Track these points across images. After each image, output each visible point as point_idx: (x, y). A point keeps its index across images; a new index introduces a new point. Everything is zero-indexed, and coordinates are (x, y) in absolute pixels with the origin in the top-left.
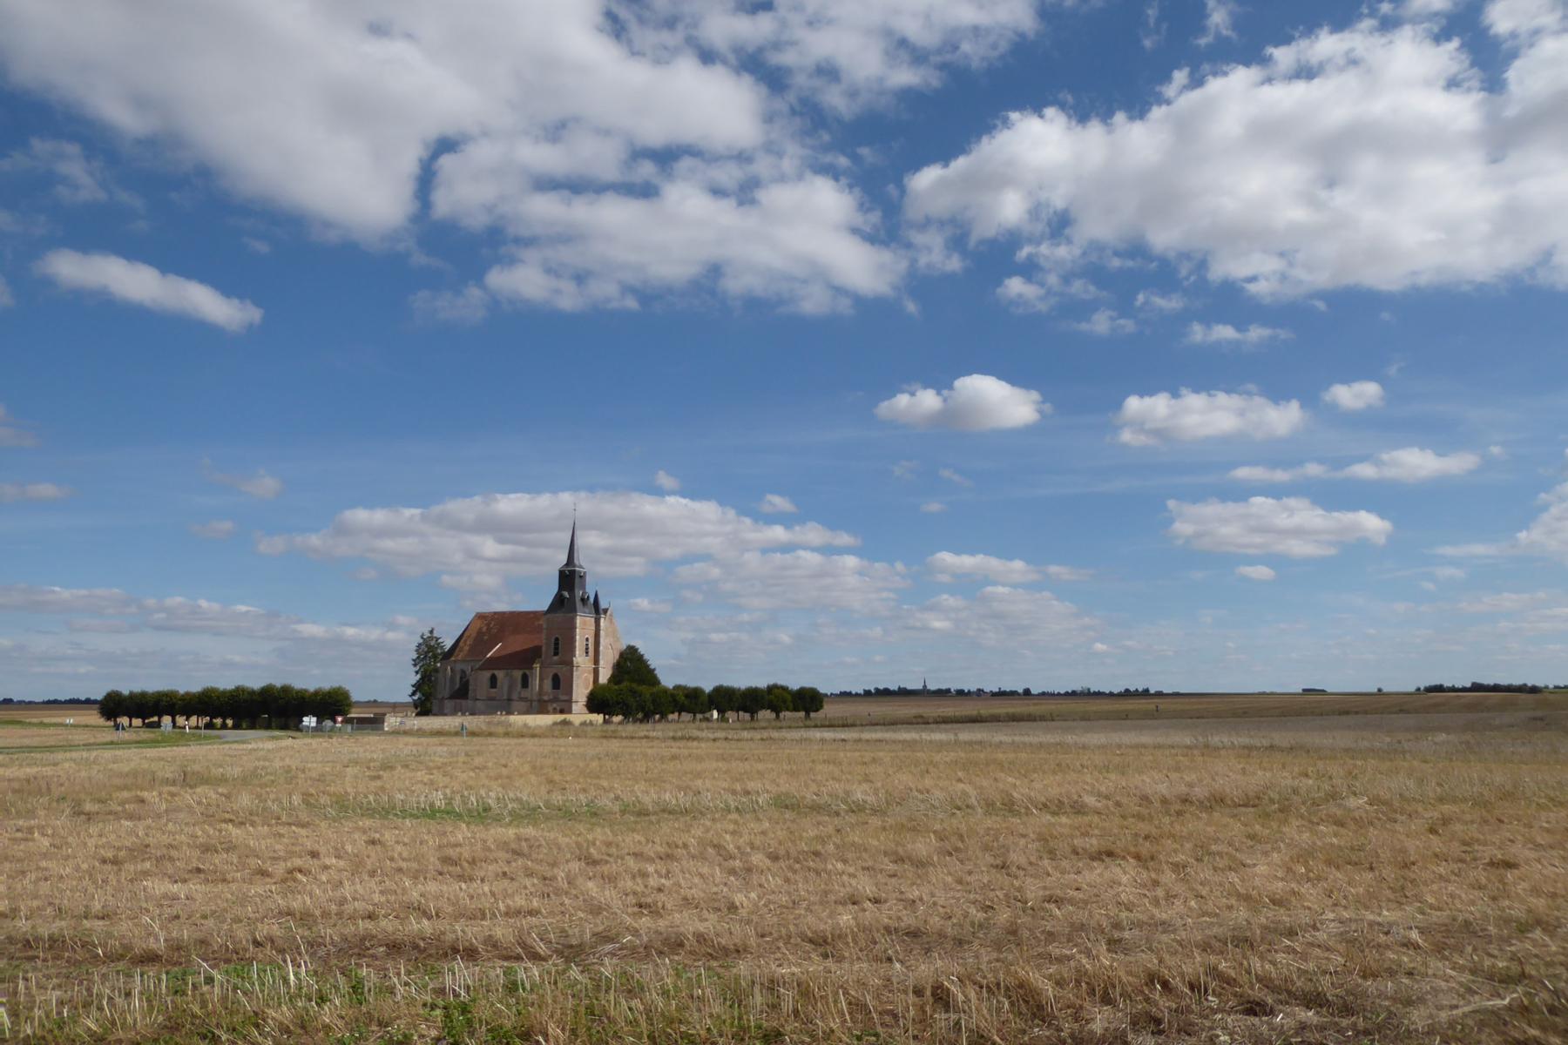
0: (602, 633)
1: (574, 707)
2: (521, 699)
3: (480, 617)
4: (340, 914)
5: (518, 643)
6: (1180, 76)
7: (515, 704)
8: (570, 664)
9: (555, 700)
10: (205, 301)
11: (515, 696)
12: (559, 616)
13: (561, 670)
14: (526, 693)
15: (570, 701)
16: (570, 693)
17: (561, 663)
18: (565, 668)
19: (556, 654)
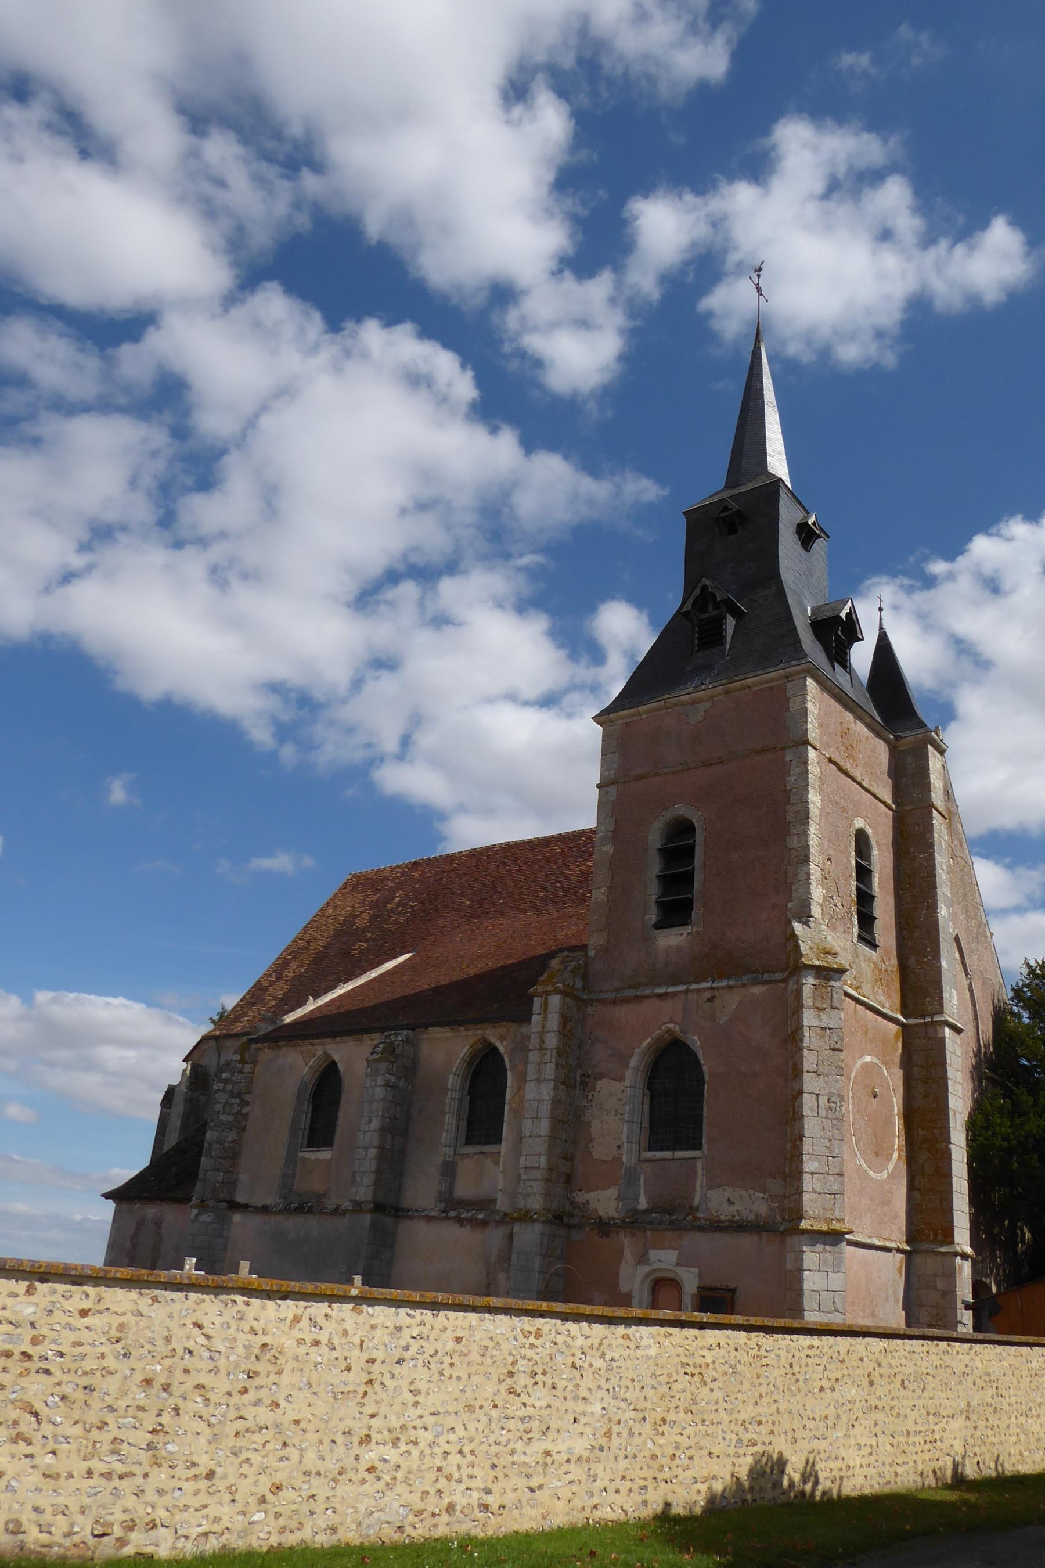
0: (880, 1019)
1: (820, 1278)
2: (455, 1208)
3: (359, 884)
4: (967, 1411)
5: (473, 949)
6: (698, 1510)
7: (428, 1239)
8: (781, 966)
9: (672, 1216)
10: (289, 1018)
11: (422, 1190)
12: (699, 699)
13: (712, 1018)
14: (487, 1175)
15: (783, 1227)
16: (781, 1161)
17: (721, 964)
18: (733, 999)
19: (675, 910)
